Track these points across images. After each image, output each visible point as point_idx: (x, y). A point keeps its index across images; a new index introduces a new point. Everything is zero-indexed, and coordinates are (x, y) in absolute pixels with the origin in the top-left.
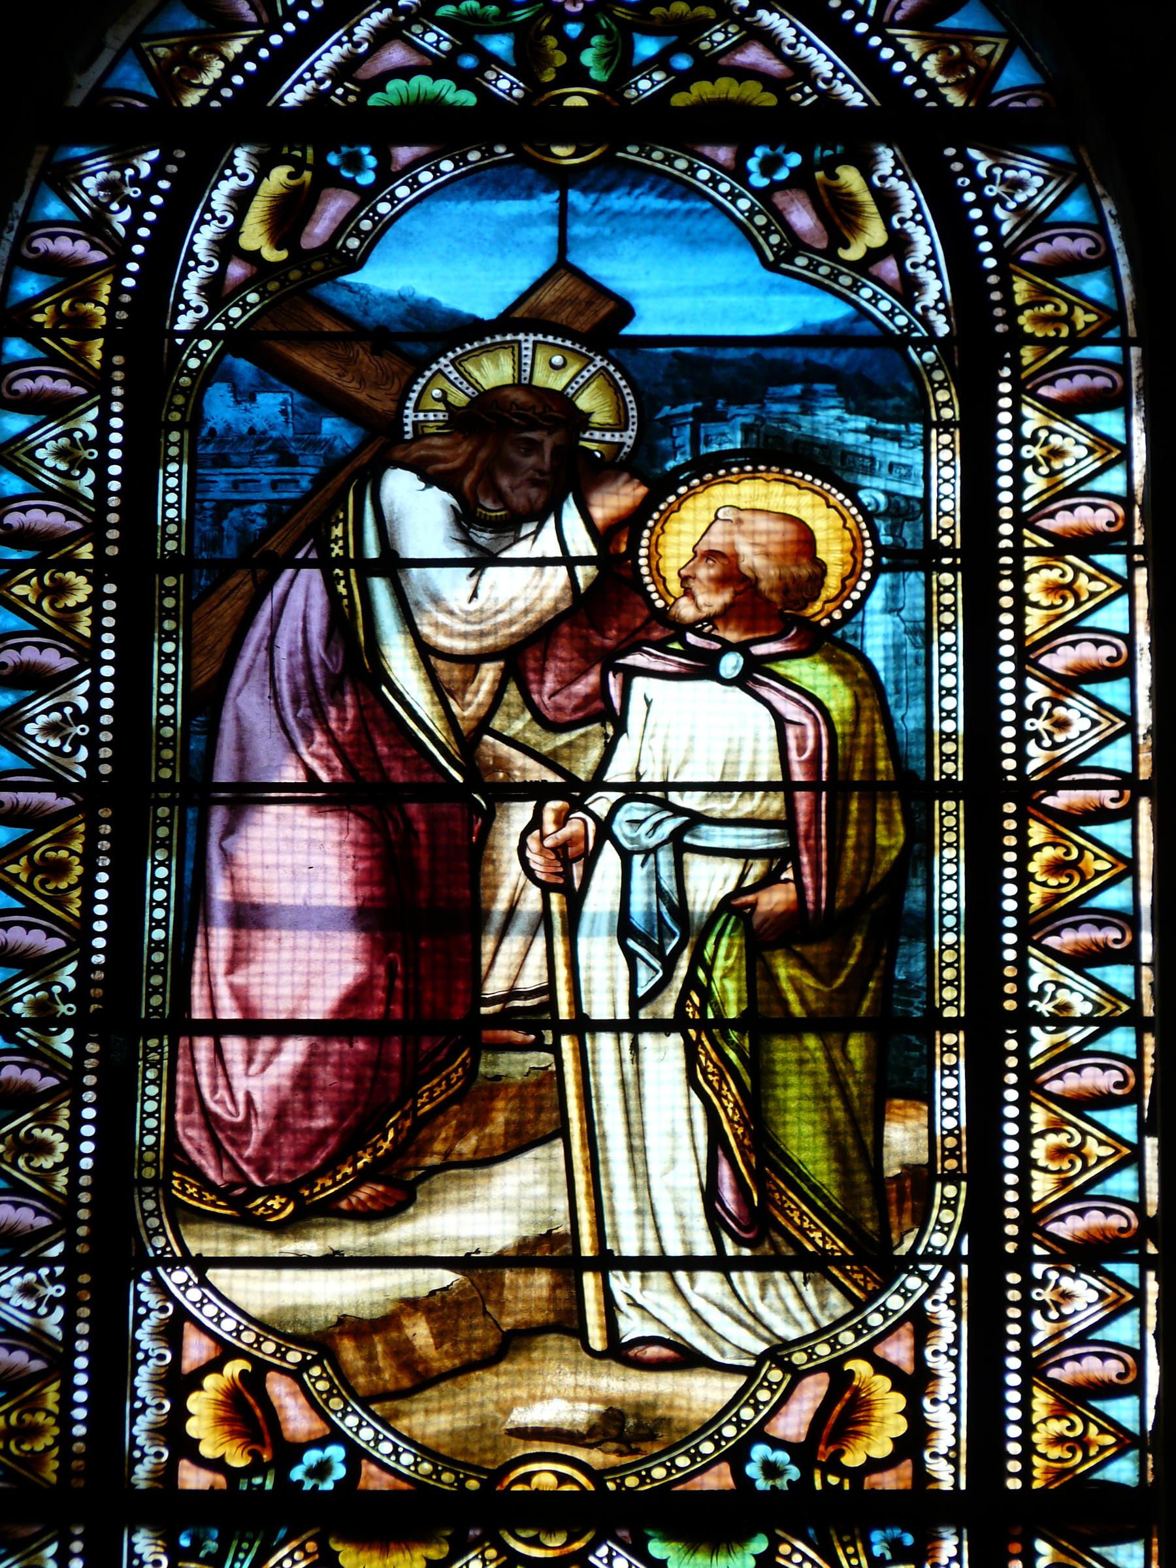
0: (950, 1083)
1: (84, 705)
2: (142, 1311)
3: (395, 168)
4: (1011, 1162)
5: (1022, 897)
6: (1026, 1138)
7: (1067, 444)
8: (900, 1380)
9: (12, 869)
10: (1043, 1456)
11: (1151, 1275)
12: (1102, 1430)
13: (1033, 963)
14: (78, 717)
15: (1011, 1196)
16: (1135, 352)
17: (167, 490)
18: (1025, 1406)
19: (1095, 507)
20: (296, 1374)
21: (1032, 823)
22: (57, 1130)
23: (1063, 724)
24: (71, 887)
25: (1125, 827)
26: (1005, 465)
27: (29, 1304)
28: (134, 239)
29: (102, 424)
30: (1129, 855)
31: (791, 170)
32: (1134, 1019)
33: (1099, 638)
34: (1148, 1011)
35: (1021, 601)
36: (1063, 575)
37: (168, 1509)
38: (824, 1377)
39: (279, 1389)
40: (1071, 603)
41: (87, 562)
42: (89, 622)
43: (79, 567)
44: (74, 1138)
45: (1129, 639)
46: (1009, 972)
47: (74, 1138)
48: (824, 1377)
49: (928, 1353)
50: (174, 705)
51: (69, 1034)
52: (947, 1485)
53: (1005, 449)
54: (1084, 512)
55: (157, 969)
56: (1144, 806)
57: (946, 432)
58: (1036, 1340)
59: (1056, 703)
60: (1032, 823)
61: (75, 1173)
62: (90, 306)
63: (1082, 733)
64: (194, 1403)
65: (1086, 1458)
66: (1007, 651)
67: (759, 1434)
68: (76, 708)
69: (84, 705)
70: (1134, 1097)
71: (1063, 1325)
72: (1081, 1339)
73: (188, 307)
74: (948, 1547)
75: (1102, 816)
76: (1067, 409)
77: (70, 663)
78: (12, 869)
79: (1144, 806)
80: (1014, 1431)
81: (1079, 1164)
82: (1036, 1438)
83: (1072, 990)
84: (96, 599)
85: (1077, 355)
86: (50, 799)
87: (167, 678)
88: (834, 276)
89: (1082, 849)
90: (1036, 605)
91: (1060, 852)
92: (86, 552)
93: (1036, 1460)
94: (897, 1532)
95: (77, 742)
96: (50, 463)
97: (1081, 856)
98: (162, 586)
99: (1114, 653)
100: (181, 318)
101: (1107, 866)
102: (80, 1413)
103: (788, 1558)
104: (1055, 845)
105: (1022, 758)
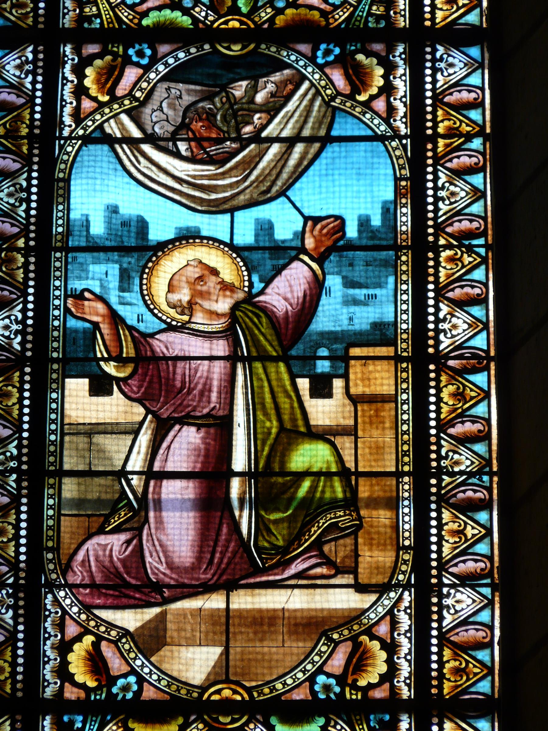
0: (404, 219)
1: (24, 184)
2: (66, 11)
3: (159, 56)
4: (434, 539)
5: (438, 411)
6: (440, 527)
7: (456, 61)
8: (384, 646)
9: (4, 6)
10: (446, 403)
11: (497, 594)
12: (473, 528)
13: (440, 174)
14: (22, 190)
15: (434, 556)
16: (496, 479)
17: (58, 218)
18: (440, 654)
19: (471, 221)
20: (115, 643)
21: (445, 648)
22: (14, 387)
23: (451, 65)
24: (14, 404)
25: (487, 652)
26: (430, 200)
27: (18, 73)
28: (16, 624)
29: (35, 52)
30: (486, 389)
31: (335, 56)
32: (481, 133)
33: (475, 419)
34: (488, 131)
35: (439, 400)
36: (459, 526)
37: (59, 706)
38: (349, 643)
39: (107, 650)
40: (465, 678)
41: (21, 249)
42: (13, 549)
43: (18, 250)
44: (17, 528)
45: (491, 628)
46: (431, 342)
47: (21, 390)
48: (349, 643)
49: (396, 634)
50: (60, 290)
51: (14, 476)
52: (405, 697)
53: (430, 192)
54: (468, 424)
55: (56, 339)
56: (493, 366)
57: (407, 552)
58: (439, 85)
59: (453, 316)
60: (445, 648)
61: (14, 682)
62: (10, 388)
63: (464, 331)
64: (71, 657)
65: (468, 679)
66: (431, 294)
67: (320, 671)
68: (21, 185)
69: (24, 184)
70: (484, 234)
71: (456, 616)
72: (457, 84)
73: (49, 684)
74: (404, 725)
75: (475, 371)
76: (460, 173)
77: (17, 166)
78: (4, 6)
79: (493, 366)
80: (434, 666)
81: (465, 678)
82: (443, 533)
83: (454, 58)
84: (26, 265)
85: (470, 481)
86: (12, 98)
87: (57, 288)
88: (353, 107)
89: (467, 662)
90: (441, 9)
91: (457, 663)
92: (21, 243)
93: (442, 405)
94: (381, 716)
95: (21, 201)
96: (6, 199)
97: (464, 389)
98: (52, 369)
99: (485, 635)
100: (47, 690)
101: (476, 394)
102: (20, 661)
103: (334, 727)
104: (455, 660)
105: (438, 342)
